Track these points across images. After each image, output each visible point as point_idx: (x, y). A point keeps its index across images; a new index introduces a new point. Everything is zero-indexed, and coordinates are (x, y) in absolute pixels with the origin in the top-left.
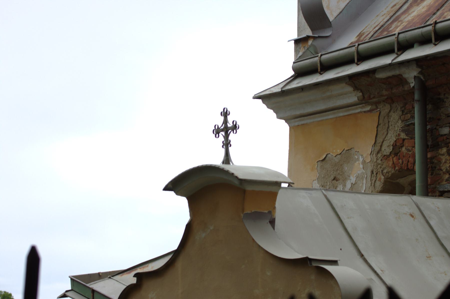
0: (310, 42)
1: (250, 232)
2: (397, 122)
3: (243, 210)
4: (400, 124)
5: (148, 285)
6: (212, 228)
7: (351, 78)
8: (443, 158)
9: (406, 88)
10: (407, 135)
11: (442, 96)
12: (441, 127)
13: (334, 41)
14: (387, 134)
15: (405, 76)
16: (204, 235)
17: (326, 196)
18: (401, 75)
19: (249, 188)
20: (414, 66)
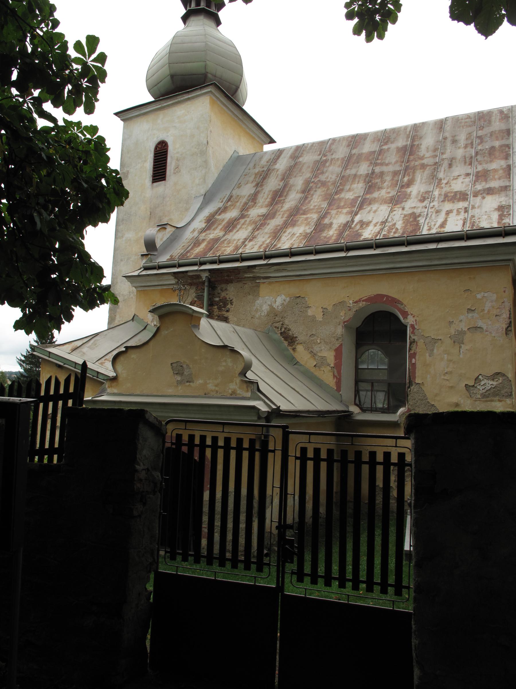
0: (149, 256)
1: (195, 333)
2: (193, 293)
3: (191, 324)
4: (194, 294)
5: (130, 351)
6: (172, 330)
7: (174, 273)
8: (215, 310)
9: (200, 280)
10: (197, 299)
11: (216, 286)
12: (215, 298)
13: (157, 258)
14: (188, 298)
15: (202, 275)
16: (166, 332)
17: (208, 321)
18: (200, 275)
19: (194, 314)
20: (208, 272)
